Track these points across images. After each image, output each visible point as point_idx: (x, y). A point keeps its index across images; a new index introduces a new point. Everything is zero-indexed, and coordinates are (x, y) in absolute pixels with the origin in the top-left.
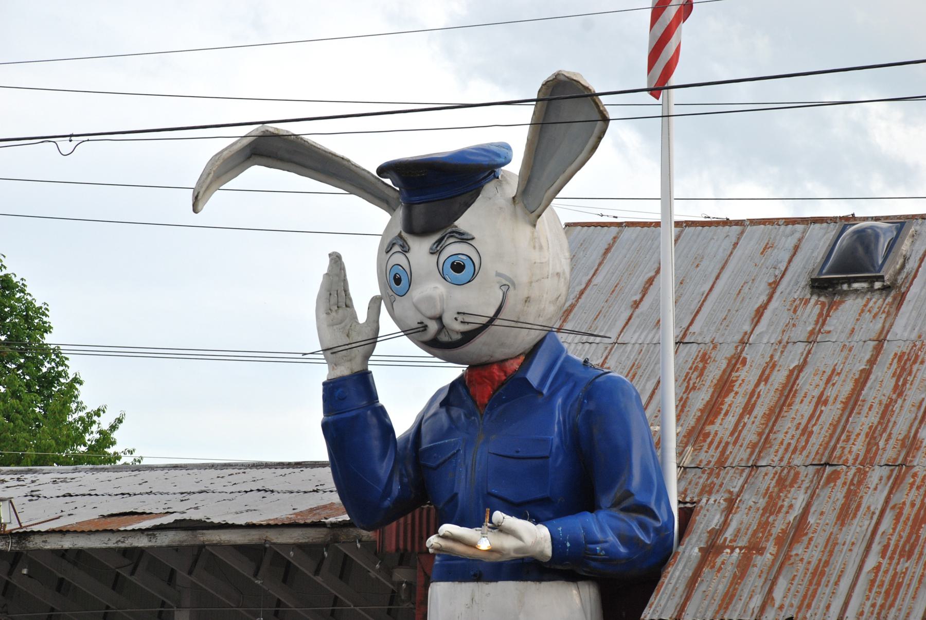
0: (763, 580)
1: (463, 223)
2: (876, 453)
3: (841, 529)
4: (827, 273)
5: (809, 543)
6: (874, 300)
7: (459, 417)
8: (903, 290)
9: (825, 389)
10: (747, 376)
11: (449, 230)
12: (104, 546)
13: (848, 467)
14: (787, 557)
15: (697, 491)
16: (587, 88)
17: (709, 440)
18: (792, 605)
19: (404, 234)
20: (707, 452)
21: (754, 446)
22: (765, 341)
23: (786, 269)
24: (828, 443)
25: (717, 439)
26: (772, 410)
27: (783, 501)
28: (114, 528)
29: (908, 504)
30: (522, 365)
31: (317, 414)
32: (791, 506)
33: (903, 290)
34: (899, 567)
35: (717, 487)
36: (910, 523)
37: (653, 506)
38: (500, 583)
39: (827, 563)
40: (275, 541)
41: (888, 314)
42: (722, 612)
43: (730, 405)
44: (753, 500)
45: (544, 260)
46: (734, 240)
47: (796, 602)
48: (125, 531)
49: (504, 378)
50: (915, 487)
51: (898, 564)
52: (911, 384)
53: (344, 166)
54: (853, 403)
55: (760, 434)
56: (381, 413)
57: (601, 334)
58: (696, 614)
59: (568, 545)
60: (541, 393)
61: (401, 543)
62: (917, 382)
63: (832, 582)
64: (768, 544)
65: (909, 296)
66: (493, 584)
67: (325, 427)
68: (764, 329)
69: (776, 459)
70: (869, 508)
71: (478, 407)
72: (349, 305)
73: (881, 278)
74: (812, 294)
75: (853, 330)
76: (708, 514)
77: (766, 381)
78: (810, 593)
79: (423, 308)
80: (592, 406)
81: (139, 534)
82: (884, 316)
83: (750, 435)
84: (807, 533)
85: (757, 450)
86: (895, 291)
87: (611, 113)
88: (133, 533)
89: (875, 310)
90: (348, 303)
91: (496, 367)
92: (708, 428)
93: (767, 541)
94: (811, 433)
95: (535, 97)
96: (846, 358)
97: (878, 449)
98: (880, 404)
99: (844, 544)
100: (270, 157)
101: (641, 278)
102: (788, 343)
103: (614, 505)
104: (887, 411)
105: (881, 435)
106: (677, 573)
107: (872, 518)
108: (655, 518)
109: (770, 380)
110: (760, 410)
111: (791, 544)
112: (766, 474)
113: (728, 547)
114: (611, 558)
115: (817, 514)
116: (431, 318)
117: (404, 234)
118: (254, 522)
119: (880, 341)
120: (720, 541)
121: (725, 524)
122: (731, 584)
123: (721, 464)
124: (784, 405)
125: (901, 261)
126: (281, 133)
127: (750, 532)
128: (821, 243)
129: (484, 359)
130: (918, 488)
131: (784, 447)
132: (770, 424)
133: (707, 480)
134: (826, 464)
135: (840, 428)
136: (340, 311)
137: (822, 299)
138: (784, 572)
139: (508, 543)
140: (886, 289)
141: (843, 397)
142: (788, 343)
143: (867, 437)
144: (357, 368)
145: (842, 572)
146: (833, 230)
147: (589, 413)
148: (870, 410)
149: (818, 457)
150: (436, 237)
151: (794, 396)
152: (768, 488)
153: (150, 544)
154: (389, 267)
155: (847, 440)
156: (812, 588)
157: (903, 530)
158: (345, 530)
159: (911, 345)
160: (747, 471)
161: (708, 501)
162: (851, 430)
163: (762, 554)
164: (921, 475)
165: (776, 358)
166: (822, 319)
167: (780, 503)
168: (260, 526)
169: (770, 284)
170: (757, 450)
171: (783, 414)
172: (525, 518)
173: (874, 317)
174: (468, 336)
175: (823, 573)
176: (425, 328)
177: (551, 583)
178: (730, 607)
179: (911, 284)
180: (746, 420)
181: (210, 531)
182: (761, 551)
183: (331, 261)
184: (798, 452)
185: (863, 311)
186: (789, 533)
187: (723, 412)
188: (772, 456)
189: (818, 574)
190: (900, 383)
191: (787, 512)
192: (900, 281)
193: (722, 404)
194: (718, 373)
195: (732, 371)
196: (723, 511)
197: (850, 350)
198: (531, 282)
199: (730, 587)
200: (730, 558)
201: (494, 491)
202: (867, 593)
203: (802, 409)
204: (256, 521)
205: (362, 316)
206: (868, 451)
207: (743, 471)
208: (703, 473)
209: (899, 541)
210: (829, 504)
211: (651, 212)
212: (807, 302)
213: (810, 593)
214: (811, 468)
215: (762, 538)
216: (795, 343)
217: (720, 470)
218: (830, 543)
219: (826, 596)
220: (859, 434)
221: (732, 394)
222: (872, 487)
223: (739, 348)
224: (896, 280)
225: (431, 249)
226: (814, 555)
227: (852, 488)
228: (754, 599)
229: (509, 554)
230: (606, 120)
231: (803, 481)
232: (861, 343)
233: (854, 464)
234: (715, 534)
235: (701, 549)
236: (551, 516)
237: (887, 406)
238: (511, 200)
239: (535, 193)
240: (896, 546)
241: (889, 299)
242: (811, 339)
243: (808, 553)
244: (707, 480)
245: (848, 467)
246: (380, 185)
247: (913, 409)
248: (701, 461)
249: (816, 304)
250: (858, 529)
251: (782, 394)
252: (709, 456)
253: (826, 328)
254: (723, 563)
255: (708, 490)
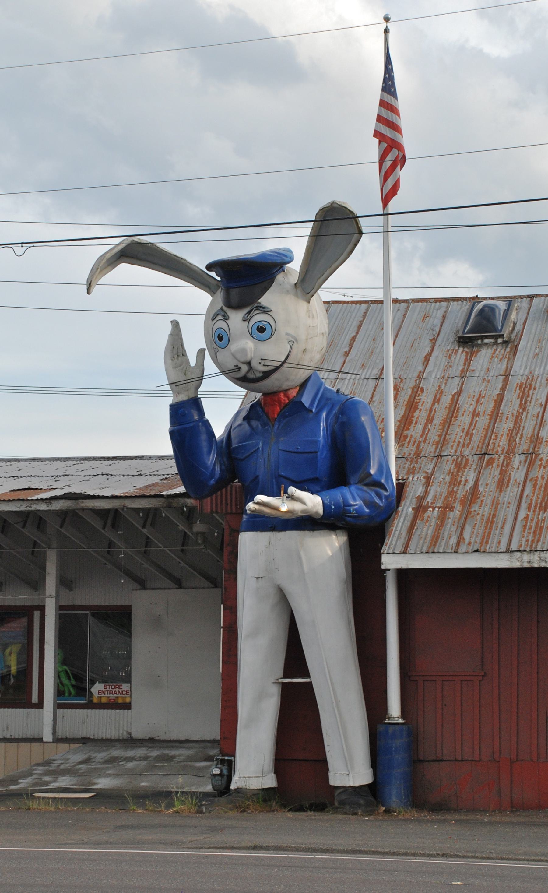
0: (455, 527)
1: (264, 301)
2: (515, 446)
3: (500, 494)
4: (467, 333)
5: (482, 504)
6: (499, 350)
7: (257, 426)
8: (516, 343)
9: (476, 406)
10: (426, 399)
11: (256, 305)
12: (18, 509)
13: (499, 455)
14: (469, 512)
15: (405, 472)
16: (352, 212)
17: (408, 440)
18: (476, 542)
19: (224, 308)
20: (407, 447)
21: (438, 443)
22: (433, 376)
23: (440, 331)
24: (484, 440)
25: (413, 439)
26: (445, 420)
27: (461, 477)
28: (25, 498)
29: (540, 477)
30: (298, 393)
31: (165, 425)
32: (466, 481)
33: (516, 343)
34: (540, 517)
35: (417, 470)
36: (543, 489)
37: (383, 481)
38: (287, 532)
39: (494, 516)
40: (130, 506)
41: (509, 359)
42: (432, 547)
43: (418, 418)
44: (441, 478)
45: (315, 325)
46: (404, 312)
47: (478, 540)
48: (32, 500)
49: (287, 401)
50: (542, 467)
51: (539, 515)
52: (530, 403)
53: (182, 263)
54: (495, 415)
55: (440, 436)
56: (207, 424)
57: (355, 373)
58: (416, 549)
59: (333, 507)
60: (311, 411)
61: (214, 506)
62: (533, 401)
63: (499, 527)
64: (456, 505)
65: (520, 347)
66: (283, 533)
67: (172, 434)
68: (432, 369)
69: (452, 451)
70: (516, 480)
71: (270, 420)
72: (184, 354)
73: (502, 336)
74: (459, 347)
75: (488, 369)
76: (414, 487)
77: (438, 401)
78: (486, 534)
79: (238, 356)
80: (345, 419)
81: (41, 502)
82: (506, 360)
83: (433, 435)
84: (479, 498)
85: (440, 446)
86: (511, 345)
87: (364, 230)
88: (37, 502)
89: (501, 356)
90: (184, 353)
91: (282, 394)
92: (406, 433)
93: (455, 502)
94: (472, 434)
95: (314, 219)
96: (487, 387)
97: (516, 443)
98: (513, 415)
99: (504, 504)
100: (132, 257)
101: (347, 337)
102: (448, 378)
103: (359, 482)
104: (517, 420)
105: (516, 435)
106: (400, 524)
107: (518, 487)
108: (386, 490)
109: (441, 402)
110: (437, 421)
111: (470, 504)
112: (448, 461)
113: (430, 507)
114: (359, 515)
115: (484, 485)
116: (243, 363)
117: (224, 308)
118: (116, 494)
119: (507, 376)
120: (425, 503)
121: (426, 493)
122: (436, 530)
123: (418, 455)
124: (452, 417)
125: (512, 325)
126: (142, 242)
127: (443, 497)
128: (460, 314)
129: (275, 389)
130: (545, 467)
131: (456, 444)
132: (446, 429)
133: (410, 465)
134: (485, 454)
135: (490, 431)
136: (180, 358)
137: (466, 349)
138: (468, 521)
139: (297, 507)
140: (505, 343)
141: (489, 411)
142: (448, 378)
143: (508, 436)
144: (192, 395)
145: (505, 520)
146: (467, 306)
147: (343, 423)
148: (507, 419)
149: (479, 449)
150: (247, 310)
151: (457, 411)
152: (450, 469)
153: (48, 508)
154: (214, 330)
155: (496, 438)
156: (487, 531)
157: (539, 494)
158: (176, 500)
159: (526, 379)
160: (435, 459)
161: (413, 478)
162: (497, 432)
163: (453, 511)
164: (545, 459)
165: (443, 387)
166: (468, 362)
167: (459, 479)
168: (121, 497)
169: (431, 340)
170: (440, 446)
171: (452, 423)
172: (305, 490)
173: (501, 360)
174: (267, 374)
175: (492, 522)
176: (239, 369)
177: (320, 531)
178: (438, 544)
179: (520, 339)
180: (429, 427)
181: (88, 500)
182: (452, 509)
183: (173, 327)
184: (466, 447)
185: (492, 357)
186: (468, 497)
187: (414, 422)
188: (450, 450)
189: (490, 522)
190: (523, 402)
191: (465, 485)
192: (513, 338)
193: (413, 417)
194: (407, 397)
195: (415, 396)
196: (423, 485)
197: (488, 382)
198: (307, 339)
199: (435, 532)
200: (433, 514)
201: (283, 474)
202: (523, 533)
203: (464, 420)
204: (116, 493)
205: (193, 362)
206: (509, 445)
207: (432, 459)
208: (407, 460)
209: (537, 501)
210: (491, 479)
211: (378, 295)
212: (457, 352)
213: (486, 534)
214: (476, 456)
215: (451, 501)
216: (453, 378)
217: (418, 459)
218: (495, 503)
219: (497, 536)
220: (503, 435)
221: (418, 411)
222: (516, 467)
223: (418, 381)
224: (511, 337)
225: (244, 317)
226: (486, 510)
227: (503, 468)
228: (452, 539)
229: (297, 514)
230: (361, 233)
231: (472, 465)
232: (495, 377)
233: (502, 454)
234: (421, 499)
235: (413, 509)
236: (319, 489)
237: (517, 417)
238: (294, 285)
239: (308, 284)
240: (536, 504)
241: (508, 349)
242: (463, 375)
243: (482, 509)
244: (410, 465)
245: (499, 455)
246: (205, 276)
247: (534, 418)
248: (405, 453)
249: (462, 353)
250: (511, 494)
251: (449, 410)
252: (409, 450)
253: (471, 368)
254: (429, 517)
255: (412, 471)
